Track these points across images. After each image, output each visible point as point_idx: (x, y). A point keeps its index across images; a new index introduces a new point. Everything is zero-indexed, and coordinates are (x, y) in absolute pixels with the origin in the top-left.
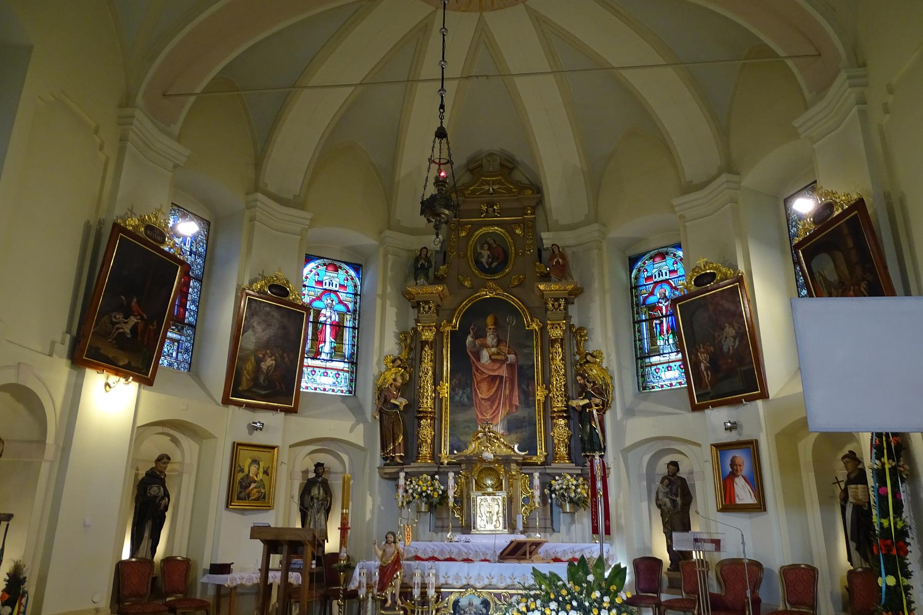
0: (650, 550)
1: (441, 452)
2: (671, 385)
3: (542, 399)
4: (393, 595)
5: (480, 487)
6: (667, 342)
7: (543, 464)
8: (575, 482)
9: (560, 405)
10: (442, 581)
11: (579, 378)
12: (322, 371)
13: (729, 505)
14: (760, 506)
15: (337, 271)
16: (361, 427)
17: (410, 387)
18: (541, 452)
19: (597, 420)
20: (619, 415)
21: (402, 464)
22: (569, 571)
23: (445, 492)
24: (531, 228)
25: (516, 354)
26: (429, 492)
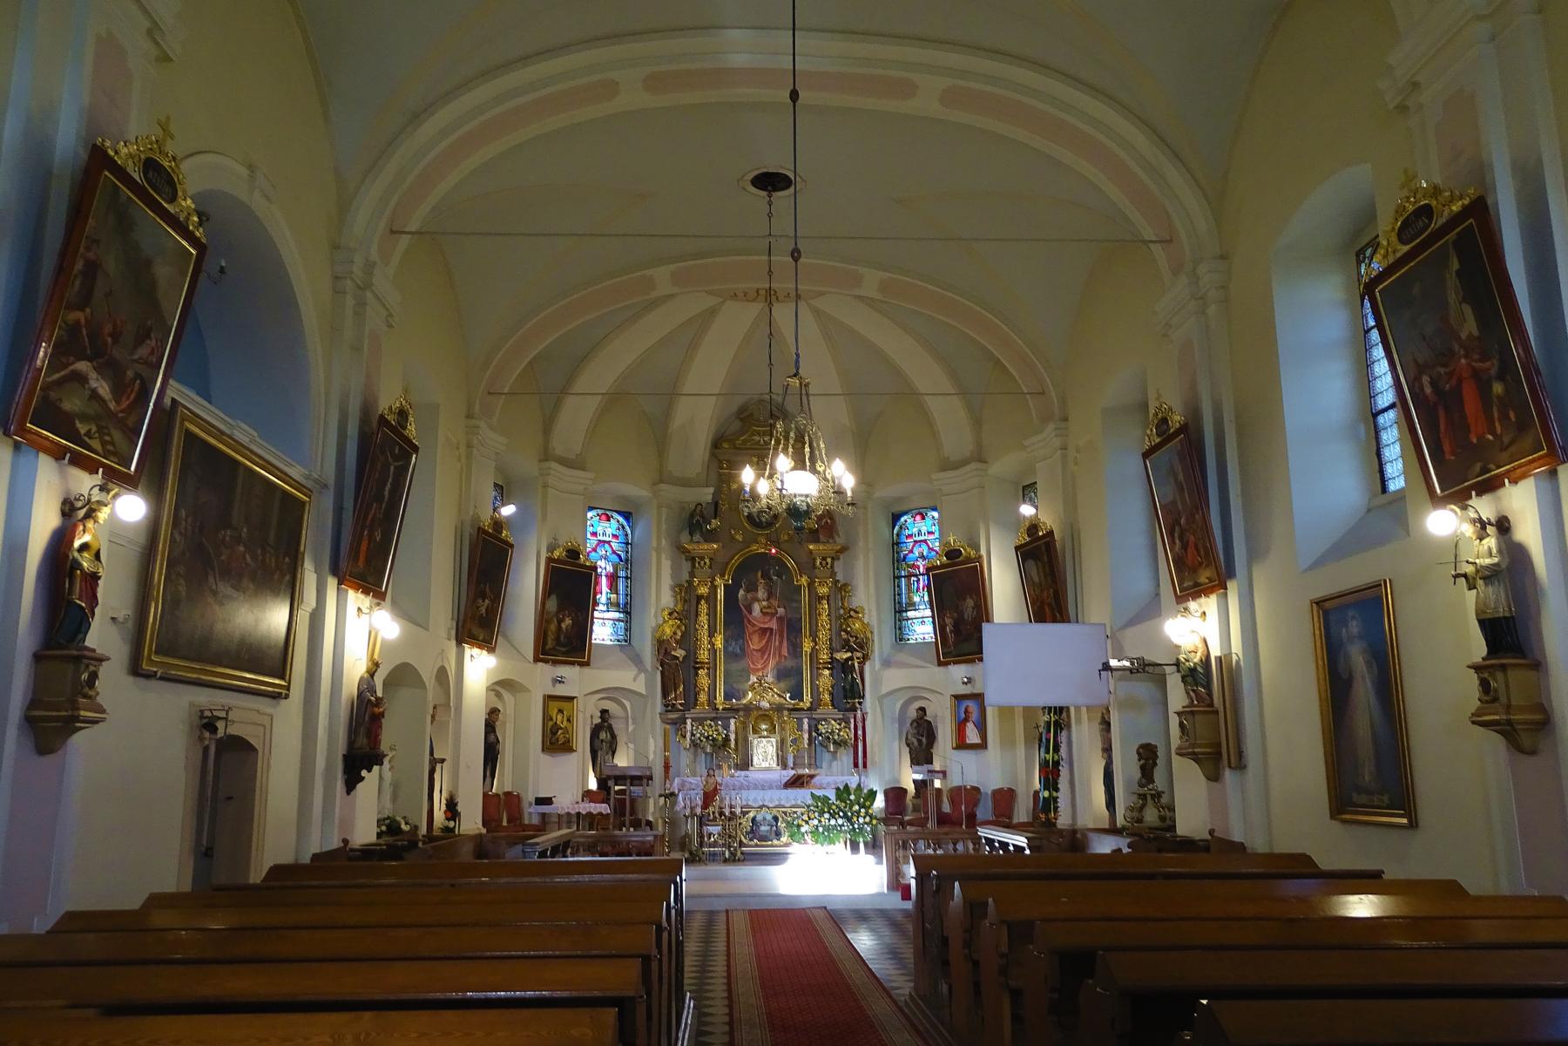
0: (899, 782)
1: (716, 698)
2: (924, 638)
3: (809, 651)
4: (714, 813)
5: (755, 731)
6: (921, 597)
7: (809, 709)
8: (838, 727)
9: (825, 657)
10: (744, 803)
11: (843, 633)
12: (601, 621)
13: (961, 744)
14: (983, 746)
15: (609, 520)
16: (642, 676)
17: (688, 639)
18: (807, 698)
19: (858, 671)
20: (878, 666)
21: (683, 711)
22: (837, 794)
23: (727, 735)
25: (785, 608)
26: (715, 736)
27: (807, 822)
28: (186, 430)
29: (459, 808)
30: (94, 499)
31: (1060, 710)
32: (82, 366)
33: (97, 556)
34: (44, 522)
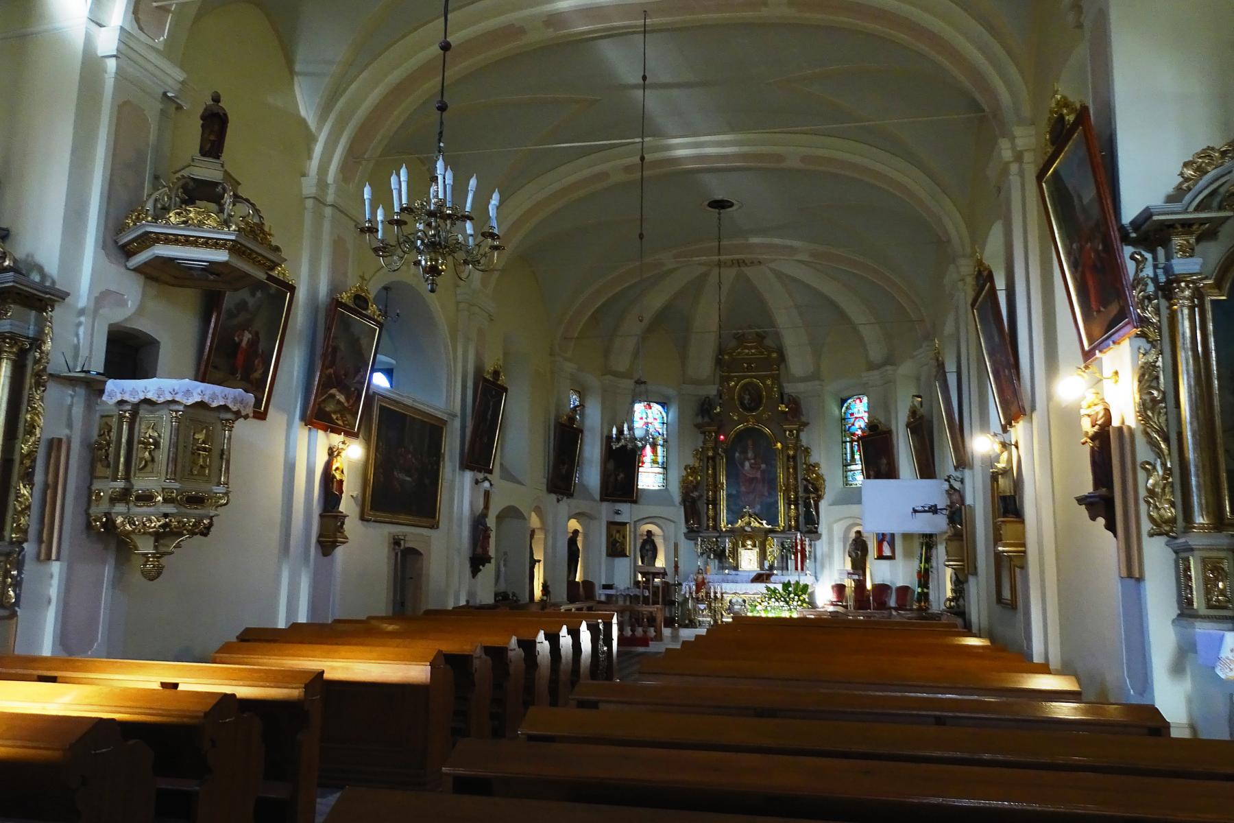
5: (744, 546)
13: (881, 557)
24: (776, 379)
27: (760, 604)
28: (382, 409)
29: (550, 589)
30: (340, 447)
31: (930, 536)
32: (333, 391)
33: (342, 472)
34: (321, 459)
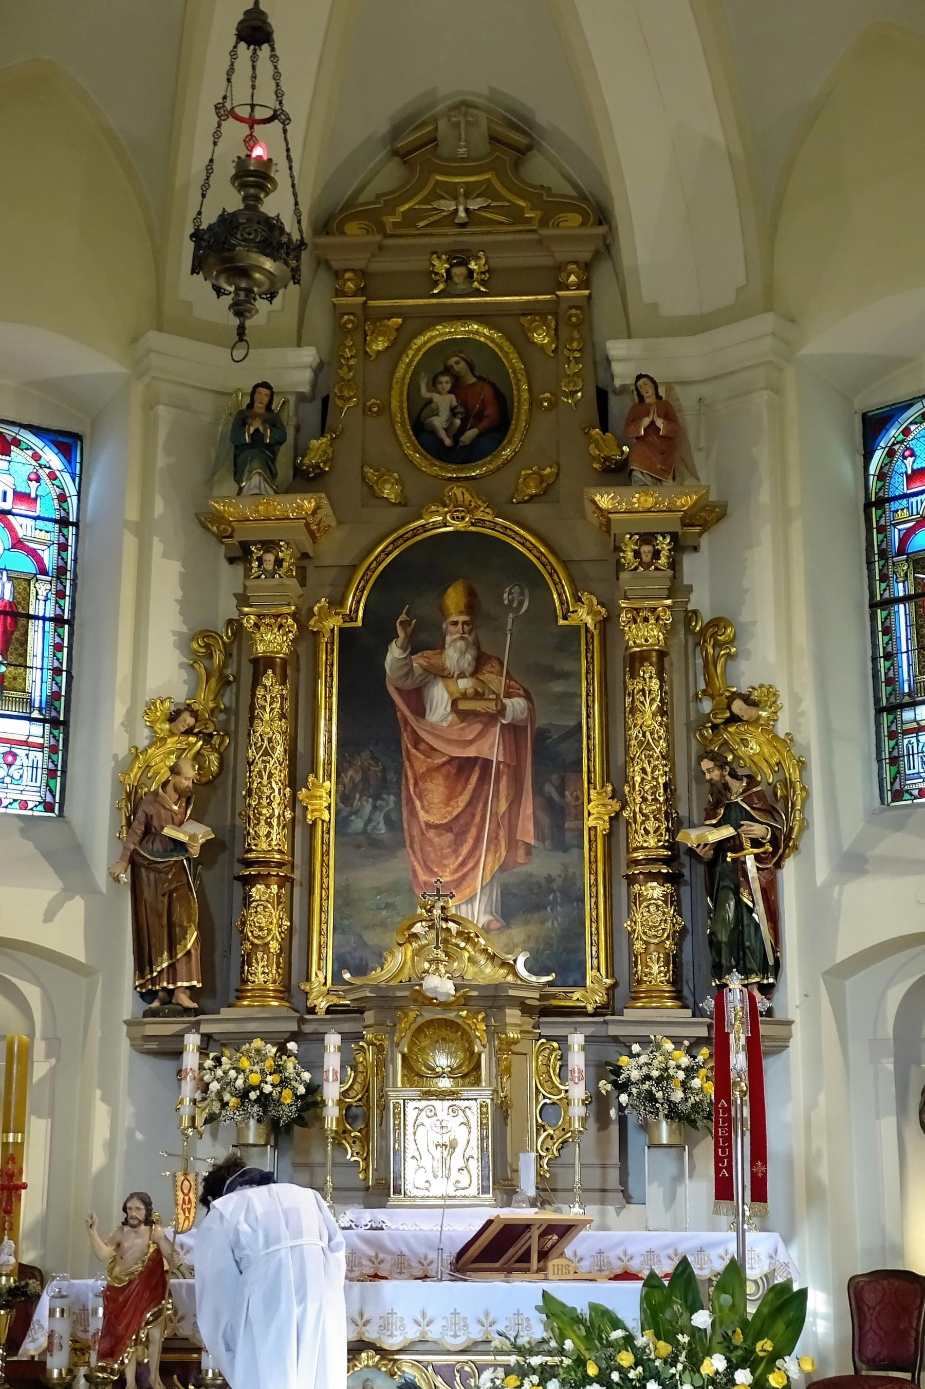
0: (899, 1251)
1: (308, 979)
3: (603, 826)
8: (685, 1061)
9: (652, 842)
11: (706, 764)
16: (76, 907)
19: (756, 886)
20: (822, 873)
21: (197, 1012)
23: (313, 1089)
25: (528, 697)
